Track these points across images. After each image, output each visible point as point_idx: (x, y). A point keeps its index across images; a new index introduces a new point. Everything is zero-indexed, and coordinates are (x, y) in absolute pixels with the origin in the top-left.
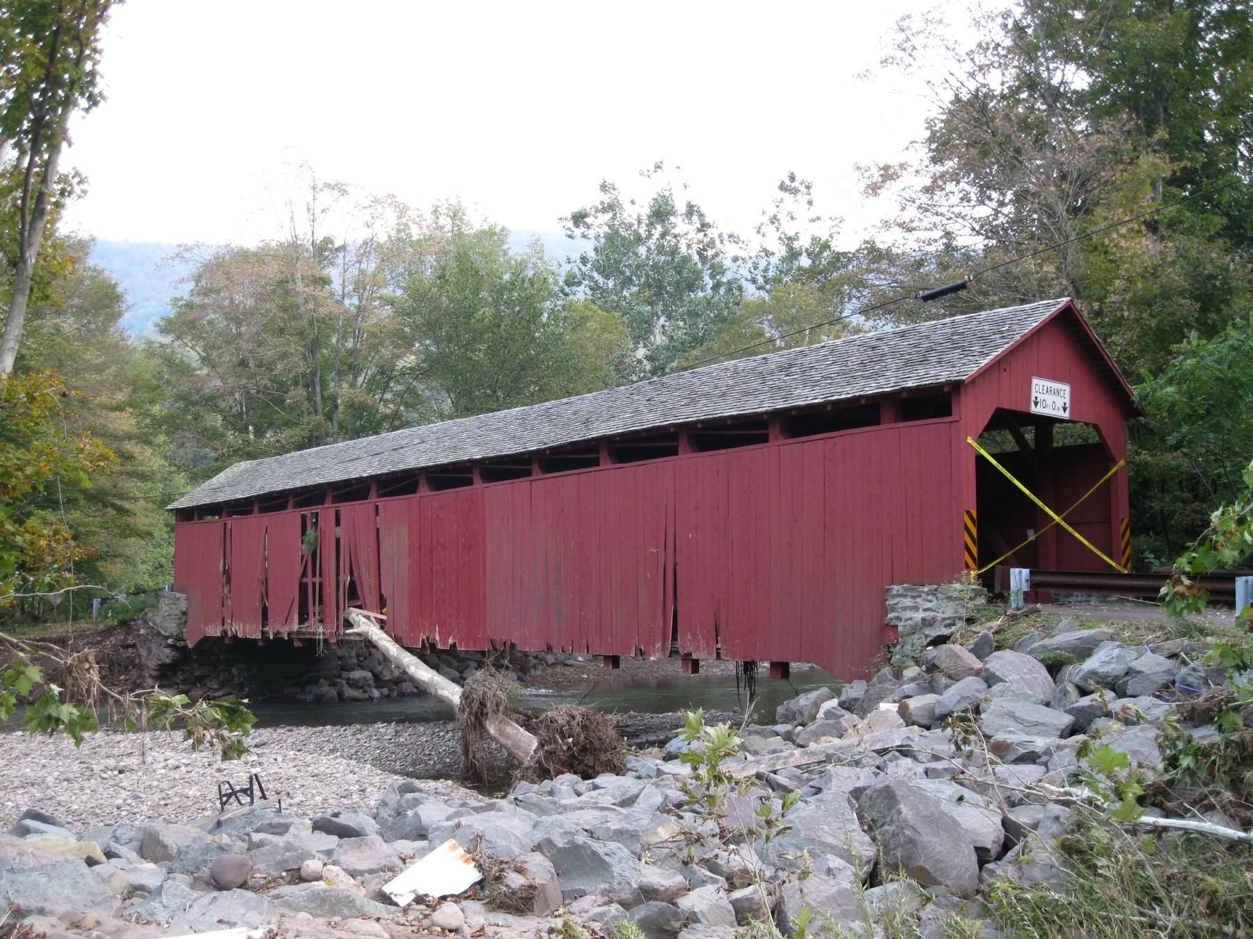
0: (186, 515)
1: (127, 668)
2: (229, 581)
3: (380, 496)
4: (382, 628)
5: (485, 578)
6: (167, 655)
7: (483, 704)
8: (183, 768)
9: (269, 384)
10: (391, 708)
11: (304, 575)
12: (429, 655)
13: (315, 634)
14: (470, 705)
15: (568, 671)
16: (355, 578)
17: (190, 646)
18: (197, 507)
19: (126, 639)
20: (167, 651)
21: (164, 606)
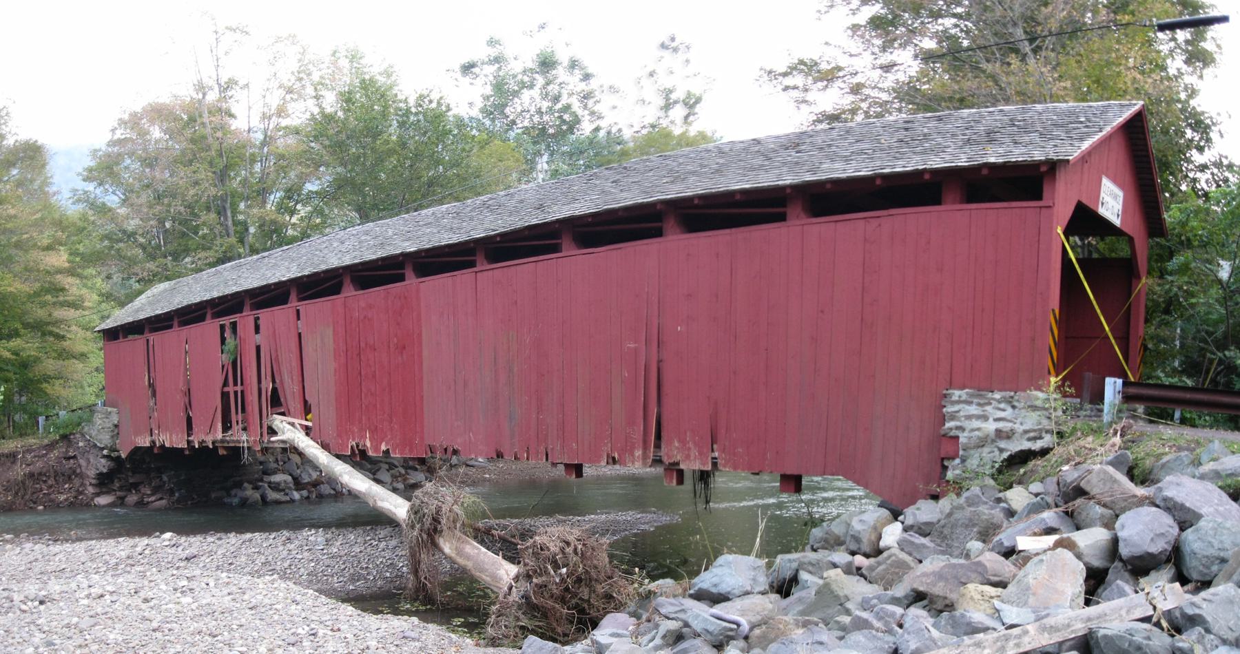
0: (111, 335)
1: (70, 477)
2: (154, 394)
3: (300, 300)
4: (307, 434)
5: (421, 379)
6: (103, 465)
7: (436, 520)
8: (107, 597)
9: (182, 209)
11: (225, 384)
12: (360, 460)
14: (420, 521)
15: (472, 471)
17: (123, 456)
18: (122, 326)
19: (67, 451)
20: (103, 461)
21: (98, 420)
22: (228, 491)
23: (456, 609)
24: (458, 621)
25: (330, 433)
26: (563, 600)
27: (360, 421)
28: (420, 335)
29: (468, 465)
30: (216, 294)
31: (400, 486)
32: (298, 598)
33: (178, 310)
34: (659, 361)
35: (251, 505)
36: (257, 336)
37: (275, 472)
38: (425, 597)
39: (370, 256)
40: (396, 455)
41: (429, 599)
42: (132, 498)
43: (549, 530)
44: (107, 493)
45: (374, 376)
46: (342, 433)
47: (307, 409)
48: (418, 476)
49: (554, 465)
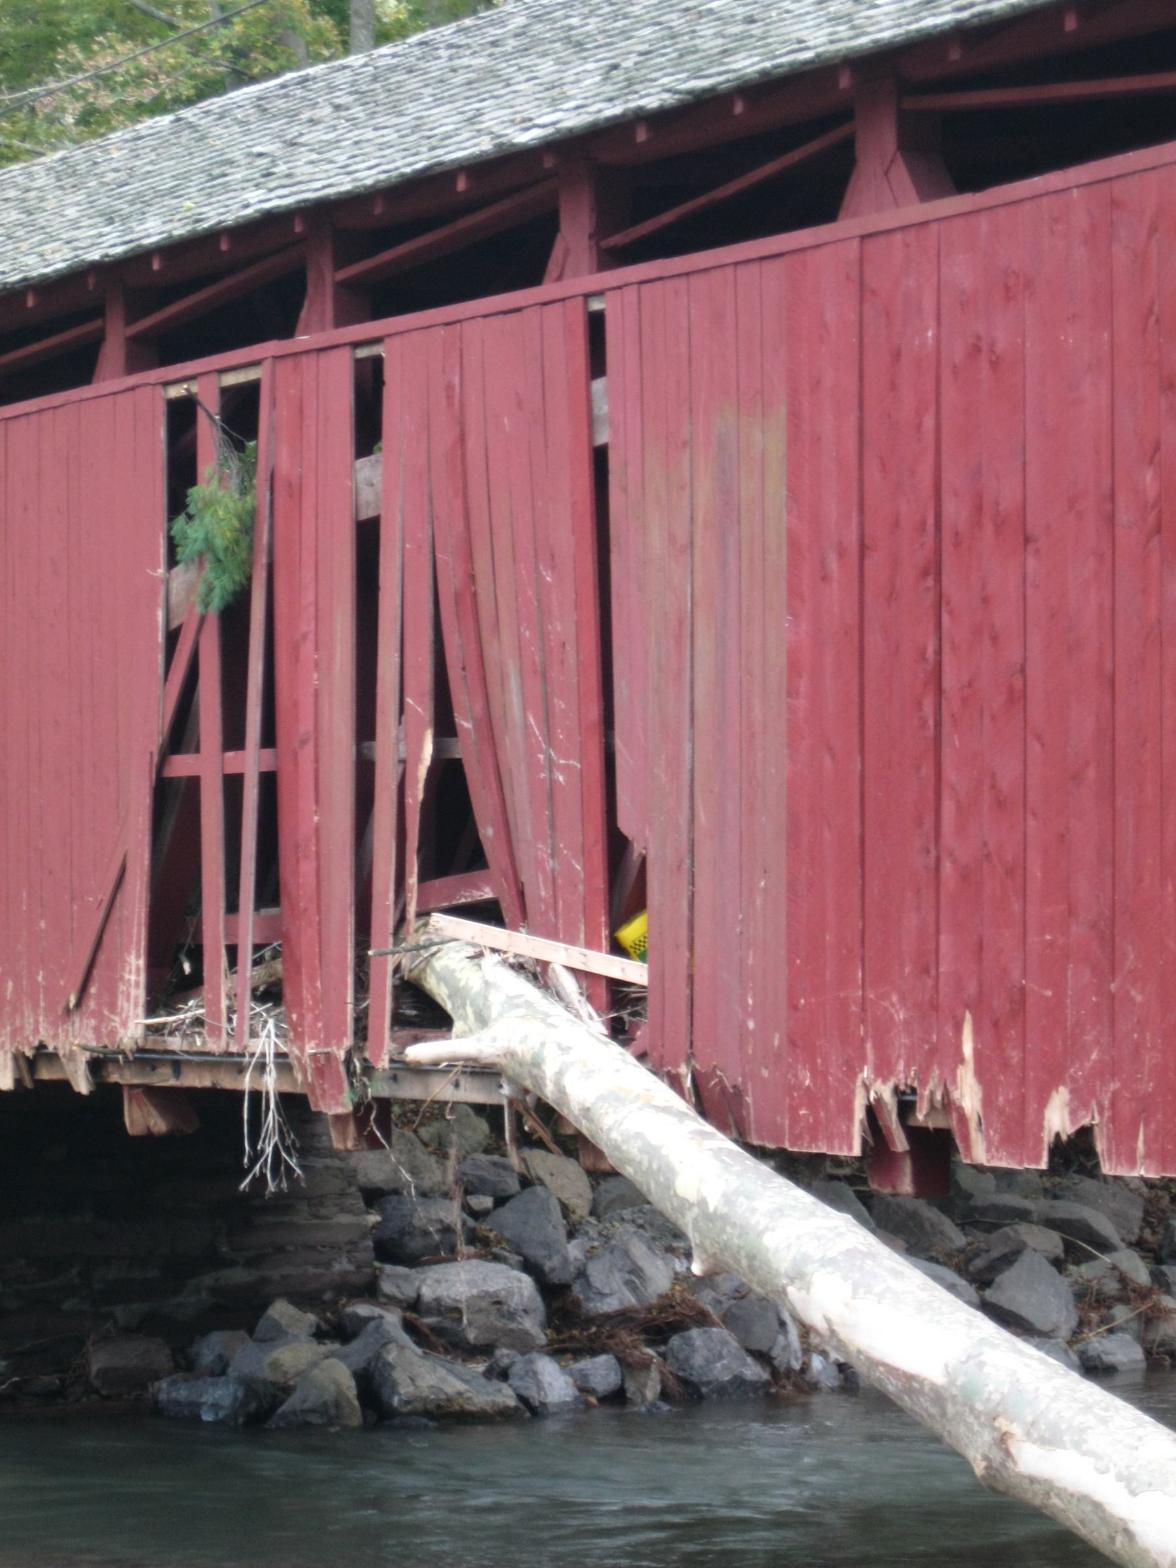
3: (613, 258)
4: (619, 1031)
11: (181, 734)
12: (913, 1186)
13: (234, 1062)
16: (464, 749)
22: (182, 1342)
25: (748, 1029)
27: (926, 966)
30: (152, 230)
31: (1123, 1351)
36: (368, 470)
37: (442, 1250)
45: (1017, 698)
46: (819, 1028)
47: (623, 888)
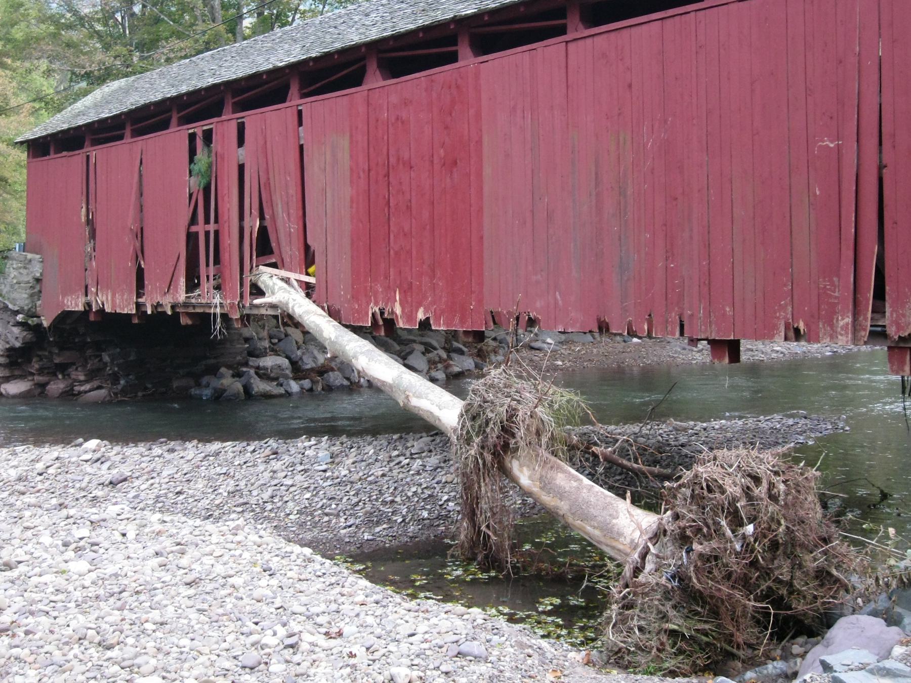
0: (38, 148)
2: (93, 235)
3: (304, 96)
4: (308, 295)
5: (480, 210)
6: (16, 336)
7: (507, 431)
10: (321, 411)
11: (193, 221)
13: (209, 306)
14: (481, 431)
16: (267, 223)
17: (46, 324)
20: (16, 330)
22: (197, 379)
23: (538, 577)
24: (548, 603)
25: (341, 295)
26: (745, 584)
27: (387, 277)
28: (479, 142)
29: (532, 348)
30: (184, 89)
31: (440, 375)
32: (275, 563)
33: (131, 112)
34: (881, 167)
35: (229, 400)
36: (241, 151)
37: (263, 354)
38: (486, 557)
39: (406, 25)
40: (439, 326)
41: (492, 562)
42: (57, 386)
43: (719, 453)
44: (22, 377)
45: (409, 208)
46: (359, 294)
47: (309, 258)
48: (466, 363)
49: (694, 341)
